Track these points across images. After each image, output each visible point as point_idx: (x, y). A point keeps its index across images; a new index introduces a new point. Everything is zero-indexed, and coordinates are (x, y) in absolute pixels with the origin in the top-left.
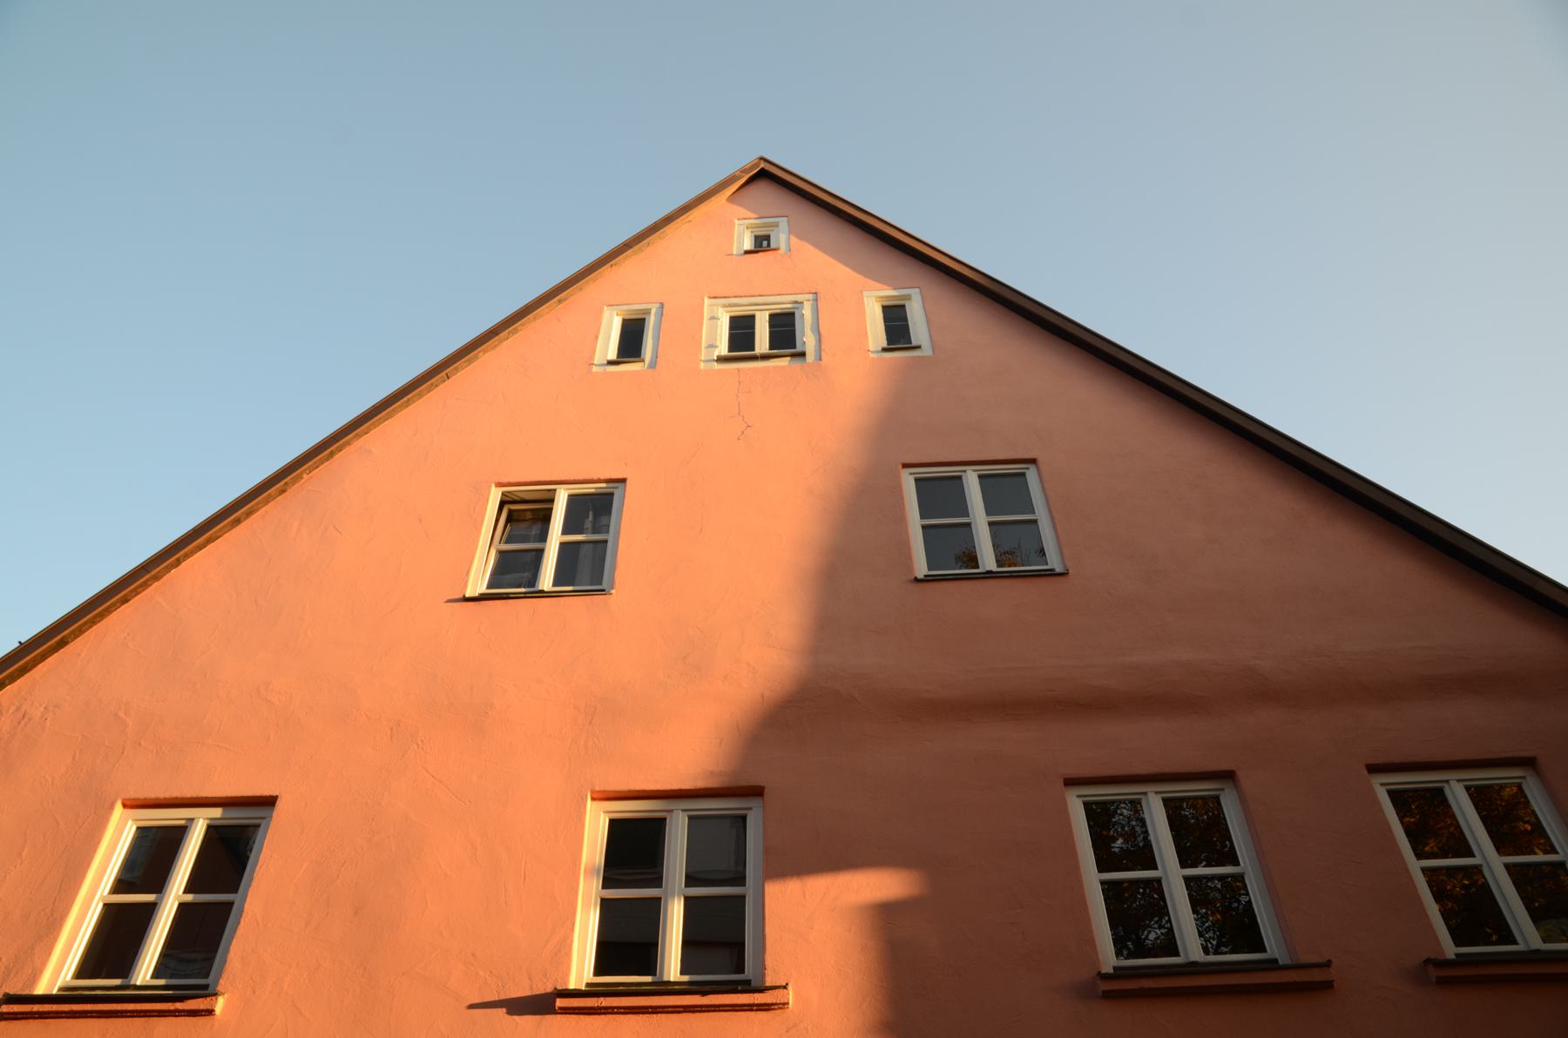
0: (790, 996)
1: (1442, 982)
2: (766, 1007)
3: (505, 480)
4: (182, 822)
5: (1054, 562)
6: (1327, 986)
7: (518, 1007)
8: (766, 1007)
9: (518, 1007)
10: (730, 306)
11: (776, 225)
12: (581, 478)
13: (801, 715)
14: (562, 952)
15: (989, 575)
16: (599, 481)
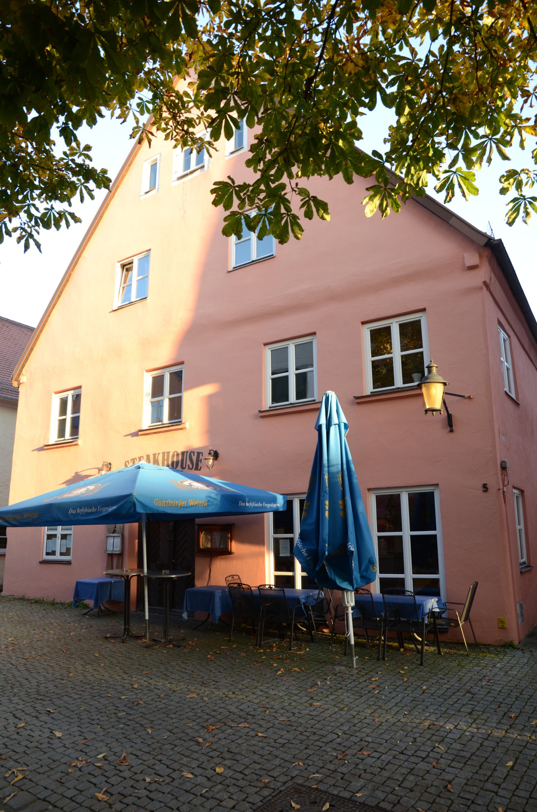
1: (358, 403)
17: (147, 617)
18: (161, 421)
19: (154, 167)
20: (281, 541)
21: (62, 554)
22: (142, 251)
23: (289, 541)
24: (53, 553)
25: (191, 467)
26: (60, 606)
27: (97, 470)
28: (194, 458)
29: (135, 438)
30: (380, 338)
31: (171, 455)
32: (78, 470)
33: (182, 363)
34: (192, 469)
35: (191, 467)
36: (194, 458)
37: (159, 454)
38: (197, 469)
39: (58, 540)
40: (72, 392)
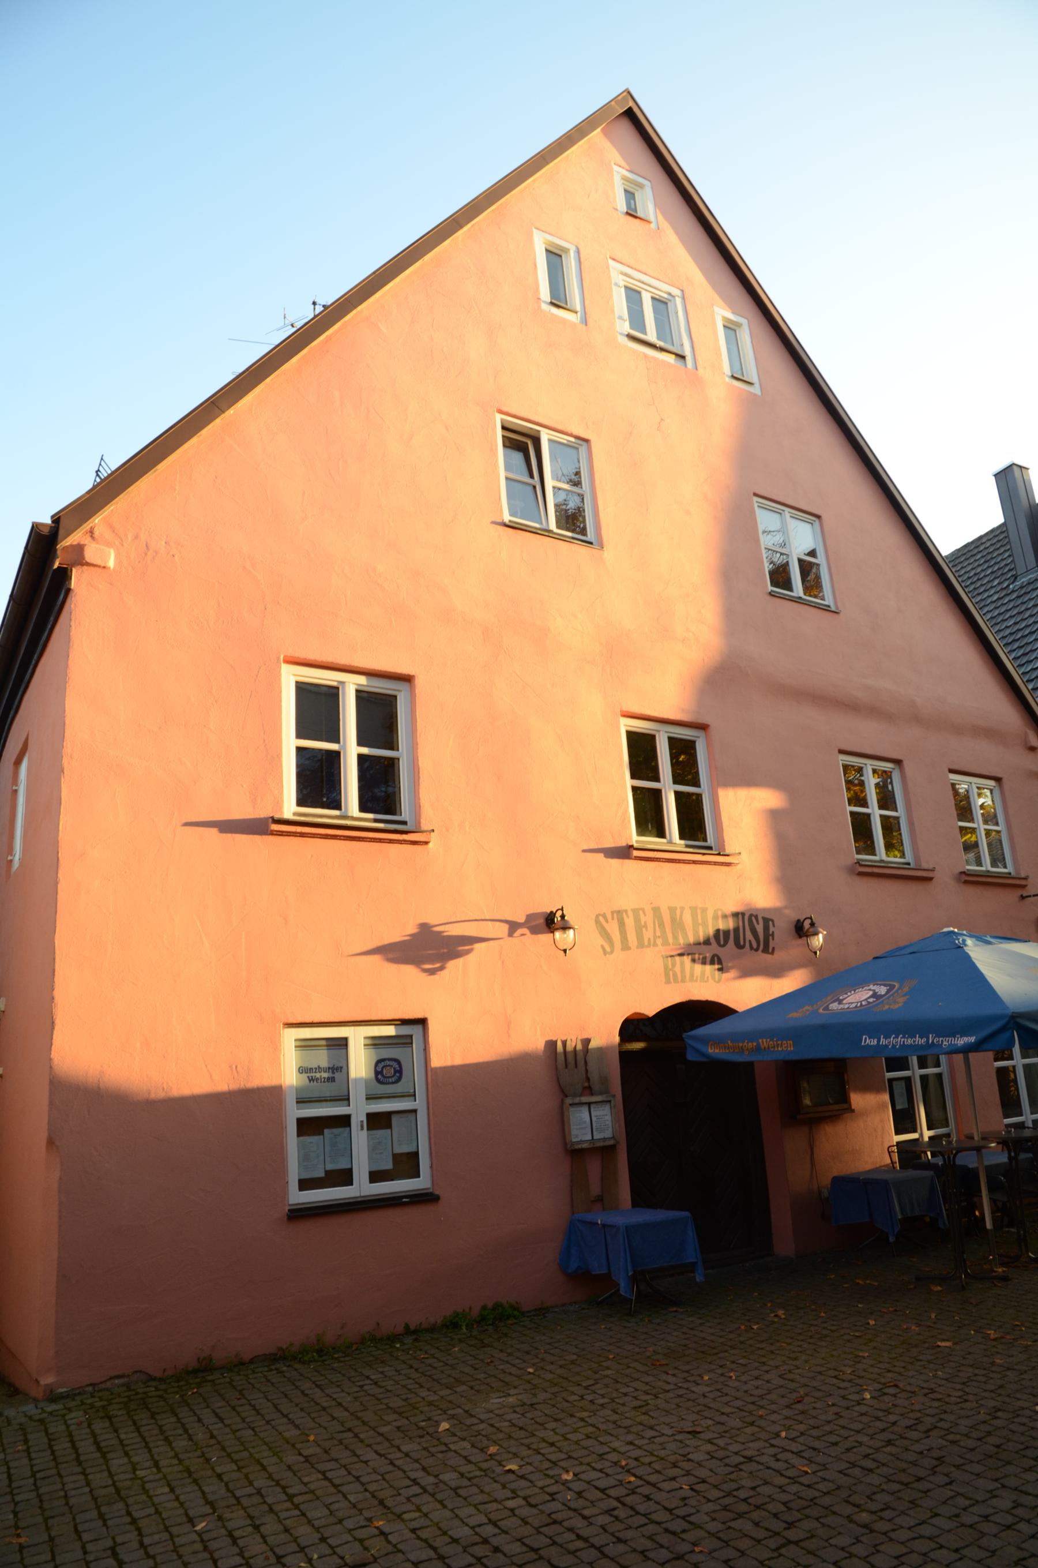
0: (434, 839)
1: (966, 882)
2: (728, 864)
3: (505, 409)
4: (335, 684)
5: (829, 600)
6: (930, 879)
7: (228, 827)
8: (728, 864)
9: (228, 827)
10: (626, 275)
11: (641, 186)
12: (559, 427)
13: (722, 678)
14: (279, 804)
15: (798, 600)
16: (571, 435)
17: (989, 1225)
18: (338, 807)
19: (555, 255)
20: (894, 1083)
21: (375, 1177)
22: (569, 430)
23: (903, 1083)
24: (345, 1177)
25: (755, 945)
26: (409, 1340)
27: (505, 927)
28: (760, 928)
29: (615, 862)
30: (317, 708)
31: (710, 914)
32: (432, 920)
33: (703, 727)
34: (757, 950)
35: (755, 945)
36: (760, 928)
37: (682, 909)
38: (766, 950)
39: (360, 1138)
40: (362, 680)
